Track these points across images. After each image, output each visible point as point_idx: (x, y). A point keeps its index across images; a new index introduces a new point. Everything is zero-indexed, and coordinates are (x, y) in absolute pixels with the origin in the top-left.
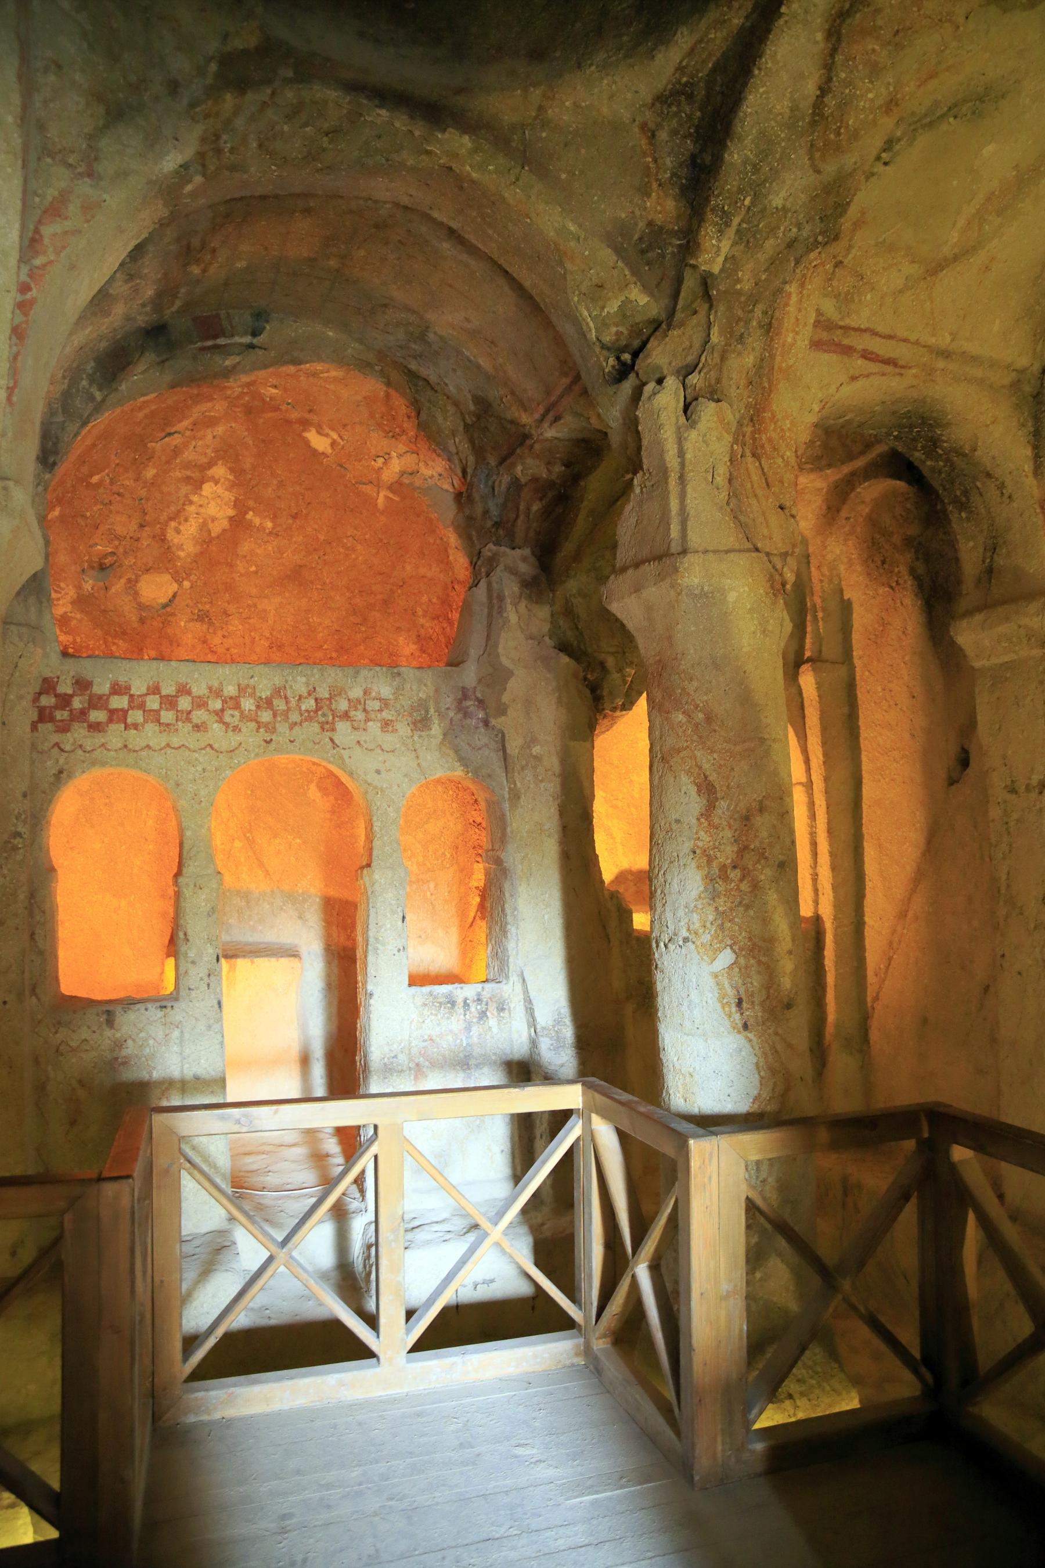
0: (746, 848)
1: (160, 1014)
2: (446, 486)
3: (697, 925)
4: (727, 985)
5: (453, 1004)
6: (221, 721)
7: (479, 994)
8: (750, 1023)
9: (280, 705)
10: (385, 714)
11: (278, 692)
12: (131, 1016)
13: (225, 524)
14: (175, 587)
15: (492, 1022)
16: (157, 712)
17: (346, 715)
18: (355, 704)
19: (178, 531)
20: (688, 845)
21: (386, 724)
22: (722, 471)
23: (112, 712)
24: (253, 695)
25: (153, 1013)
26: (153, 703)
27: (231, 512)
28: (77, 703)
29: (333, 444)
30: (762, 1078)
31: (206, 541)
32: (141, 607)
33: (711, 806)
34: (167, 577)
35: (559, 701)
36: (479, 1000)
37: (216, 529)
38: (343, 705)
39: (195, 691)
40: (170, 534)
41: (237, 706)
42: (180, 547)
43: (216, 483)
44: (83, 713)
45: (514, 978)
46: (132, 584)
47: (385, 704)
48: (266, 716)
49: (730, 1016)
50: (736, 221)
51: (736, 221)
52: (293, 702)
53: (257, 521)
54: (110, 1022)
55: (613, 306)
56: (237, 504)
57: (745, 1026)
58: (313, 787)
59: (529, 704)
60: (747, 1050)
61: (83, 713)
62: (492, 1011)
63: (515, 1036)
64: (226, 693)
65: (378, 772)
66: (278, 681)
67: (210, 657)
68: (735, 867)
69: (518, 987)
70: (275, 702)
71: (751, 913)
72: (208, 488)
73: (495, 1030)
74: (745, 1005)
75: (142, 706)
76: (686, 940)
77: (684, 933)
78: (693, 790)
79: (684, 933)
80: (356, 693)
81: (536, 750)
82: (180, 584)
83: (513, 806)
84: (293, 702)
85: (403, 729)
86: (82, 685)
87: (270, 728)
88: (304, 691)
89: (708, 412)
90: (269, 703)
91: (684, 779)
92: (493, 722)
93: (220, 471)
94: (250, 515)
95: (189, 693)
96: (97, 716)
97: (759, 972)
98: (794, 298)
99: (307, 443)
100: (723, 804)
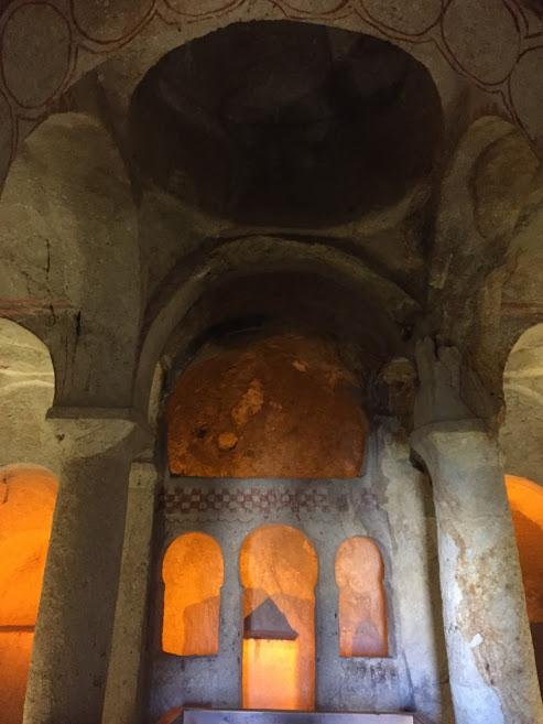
0: (484, 575)
1: (208, 664)
2: (358, 386)
3: (461, 619)
4: (479, 656)
5: (365, 669)
6: (243, 507)
7: (379, 664)
8: (495, 680)
9: (272, 499)
10: (324, 503)
11: (270, 492)
12: (194, 664)
13: (260, 407)
14: (236, 439)
15: (388, 682)
16: (213, 503)
17: (304, 504)
18: (309, 498)
19: (237, 412)
20: (453, 574)
21: (325, 508)
22: (456, 379)
23: (193, 503)
24: (258, 494)
25: (204, 664)
26: (196, 498)
27: (262, 402)
28: (177, 499)
29: (306, 368)
30: (505, 716)
31: (251, 416)
32: (220, 450)
33: (463, 552)
34: (232, 435)
35: (417, 495)
36: (379, 668)
37: (255, 410)
38: (303, 498)
39: (231, 492)
40: (234, 414)
41: (251, 499)
42: (238, 420)
43: (254, 388)
44: (179, 504)
45: (399, 656)
46: (216, 442)
47: (324, 497)
48: (265, 504)
49: (483, 675)
50: (448, 265)
51: (448, 265)
52: (278, 497)
53: (275, 405)
54: (183, 667)
55: (400, 306)
56: (264, 398)
57: (492, 682)
58: (306, 542)
59: (399, 496)
60: (494, 698)
61: (179, 504)
62: (388, 675)
63: (402, 692)
64: (185, 492)
65: (321, 533)
66: (271, 486)
67: (254, 474)
68: (479, 587)
69: (402, 662)
70: (270, 497)
71: (490, 613)
72: (250, 391)
73: (390, 688)
74: (491, 668)
75: (207, 501)
76: (456, 628)
77: (455, 624)
78: (453, 543)
79: (455, 624)
80: (309, 492)
81: (405, 522)
82: (238, 437)
83: (395, 554)
84: (278, 497)
85: (334, 510)
86: (179, 491)
87: (267, 510)
88: (283, 492)
89: (445, 352)
90: (267, 497)
91: (449, 537)
92: (382, 507)
93: (255, 383)
94: (271, 403)
95: (228, 493)
96: (186, 505)
97: (498, 650)
98: (487, 293)
99: (295, 368)
100: (469, 551)
